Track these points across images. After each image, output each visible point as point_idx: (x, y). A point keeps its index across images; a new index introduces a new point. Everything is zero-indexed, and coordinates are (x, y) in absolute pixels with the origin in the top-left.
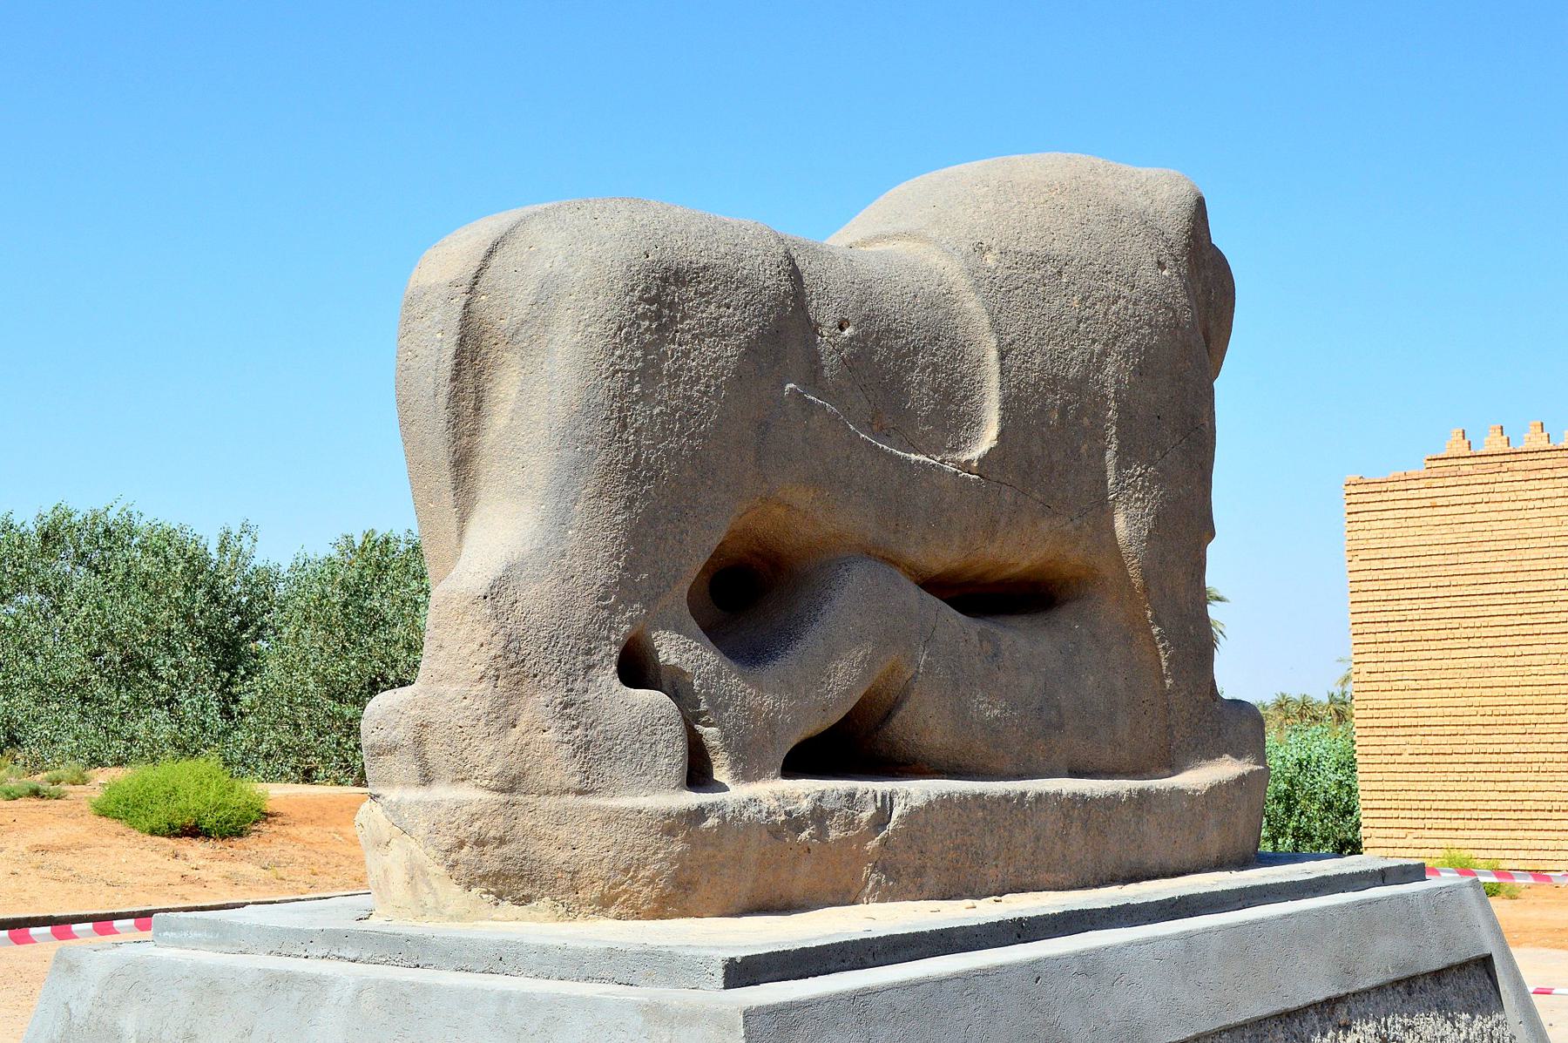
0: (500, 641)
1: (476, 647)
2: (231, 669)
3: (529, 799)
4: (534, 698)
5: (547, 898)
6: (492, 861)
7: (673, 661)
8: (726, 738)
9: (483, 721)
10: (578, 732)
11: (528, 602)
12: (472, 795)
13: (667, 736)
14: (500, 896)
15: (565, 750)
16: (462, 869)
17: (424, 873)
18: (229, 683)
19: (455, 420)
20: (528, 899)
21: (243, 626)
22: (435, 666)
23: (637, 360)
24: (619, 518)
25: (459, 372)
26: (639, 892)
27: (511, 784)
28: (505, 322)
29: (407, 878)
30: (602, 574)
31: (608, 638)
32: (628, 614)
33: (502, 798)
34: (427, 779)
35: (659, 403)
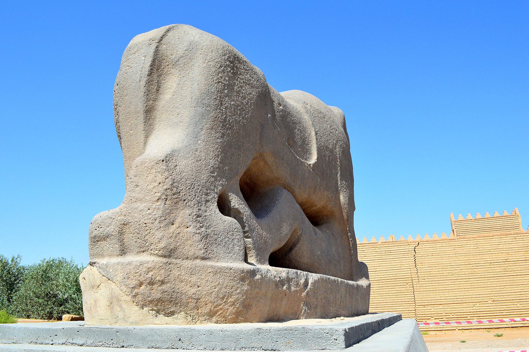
0: (169, 182)
1: (156, 184)
2: (12, 290)
3: (178, 261)
4: (183, 211)
5: (183, 313)
6: (156, 293)
7: (237, 206)
8: (254, 244)
9: (158, 221)
10: (203, 229)
11: (182, 167)
12: (148, 259)
13: (238, 237)
14: (158, 312)
15: (198, 237)
16: (140, 297)
17: (119, 300)
18: (11, 294)
19: (148, 92)
20: (172, 313)
21: (15, 280)
22: (134, 195)
23: (227, 81)
24: (219, 141)
25: (151, 74)
26: (228, 309)
27: (169, 253)
28: (173, 57)
29: (108, 303)
30: (212, 162)
31: (214, 190)
32: (221, 182)
33: (164, 260)
34: (123, 252)
35: (233, 100)
